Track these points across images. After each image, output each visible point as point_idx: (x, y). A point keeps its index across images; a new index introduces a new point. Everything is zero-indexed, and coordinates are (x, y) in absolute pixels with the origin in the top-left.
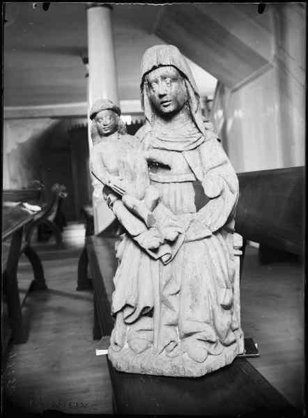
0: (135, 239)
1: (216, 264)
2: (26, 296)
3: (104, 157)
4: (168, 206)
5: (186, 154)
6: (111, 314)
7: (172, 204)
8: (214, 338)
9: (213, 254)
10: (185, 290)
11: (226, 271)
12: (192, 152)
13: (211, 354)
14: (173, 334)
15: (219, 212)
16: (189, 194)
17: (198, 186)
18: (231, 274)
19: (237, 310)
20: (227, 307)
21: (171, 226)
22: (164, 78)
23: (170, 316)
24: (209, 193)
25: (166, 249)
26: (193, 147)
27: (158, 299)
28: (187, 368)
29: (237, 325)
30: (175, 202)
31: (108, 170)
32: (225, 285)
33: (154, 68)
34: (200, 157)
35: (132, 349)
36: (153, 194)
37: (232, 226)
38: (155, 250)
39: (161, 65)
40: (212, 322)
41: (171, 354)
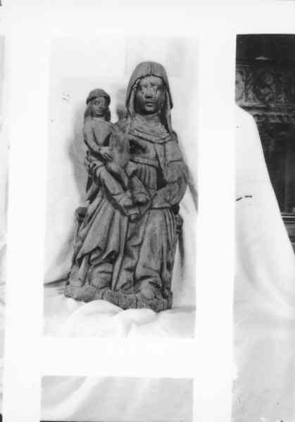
22: (153, 85)
24: (167, 177)
27: (122, 247)
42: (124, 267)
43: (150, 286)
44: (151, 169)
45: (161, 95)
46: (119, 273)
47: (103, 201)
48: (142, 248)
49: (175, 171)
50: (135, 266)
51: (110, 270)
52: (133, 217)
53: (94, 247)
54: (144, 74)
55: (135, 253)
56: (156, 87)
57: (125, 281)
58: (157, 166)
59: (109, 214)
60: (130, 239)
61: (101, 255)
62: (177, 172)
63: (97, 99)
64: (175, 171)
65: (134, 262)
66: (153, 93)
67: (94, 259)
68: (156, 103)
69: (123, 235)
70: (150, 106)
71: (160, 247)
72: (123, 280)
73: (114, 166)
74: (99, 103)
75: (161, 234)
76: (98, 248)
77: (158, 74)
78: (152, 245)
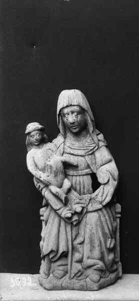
0: (57, 211)
1: (104, 224)
2: (44, 187)
3: (36, 160)
4: (75, 190)
5: (87, 157)
6: (42, 256)
7: (78, 189)
8: (104, 268)
9: (103, 219)
10: (87, 241)
11: (110, 226)
12: (90, 156)
13: (103, 278)
14: (79, 266)
15: (106, 193)
16: (87, 180)
17: (94, 176)
18: (114, 229)
19: (53, 201)
20: (111, 250)
21: (78, 203)
22: (73, 112)
23: (77, 256)
24: (100, 180)
25: (75, 218)
26: (90, 153)
27: (70, 247)
28: (92, 294)
29: (118, 260)
30: (80, 187)
31: (38, 168)
32: (110, 236)
33: (67, 106)
34: (95, 159)
35: (55, 277)
36: (67, 184)
37: (115, 200)
38: (70, 219)
39: (71, 105)
40: (102, 259)
41: (79, 278)
42: (73, 261)
43: (96, 272)
44: (85, 177)
45: (81, 117)
46: (71, 265)
47: (51, 213)
48: (85, 245)
49: (65, 281)
50: (83, 258)
51: (66, 263)
52: (75, 223)
53: (50, 251)
54: (65, 105)
55: (80, 249)
56: (75, 114)
57: (76, 272)
58: (91, 172)
59: (53, 239)
60: (75, 239)
61: (56, 255)
62: (66, 282)
63: (32, 134)
64: (65, 281)
65: (81, 255)
66: (75, 119)
67: (52, 258)
68: (79, 124)
69: (70, 238)
70: (75, 129)
71: (99, 242)
72: (74, 271)
73: (54, 189)
74: (34, 136)
75: (97, 231)
76: (52, 251)
77: (76, 104)
78: (92, 242)
